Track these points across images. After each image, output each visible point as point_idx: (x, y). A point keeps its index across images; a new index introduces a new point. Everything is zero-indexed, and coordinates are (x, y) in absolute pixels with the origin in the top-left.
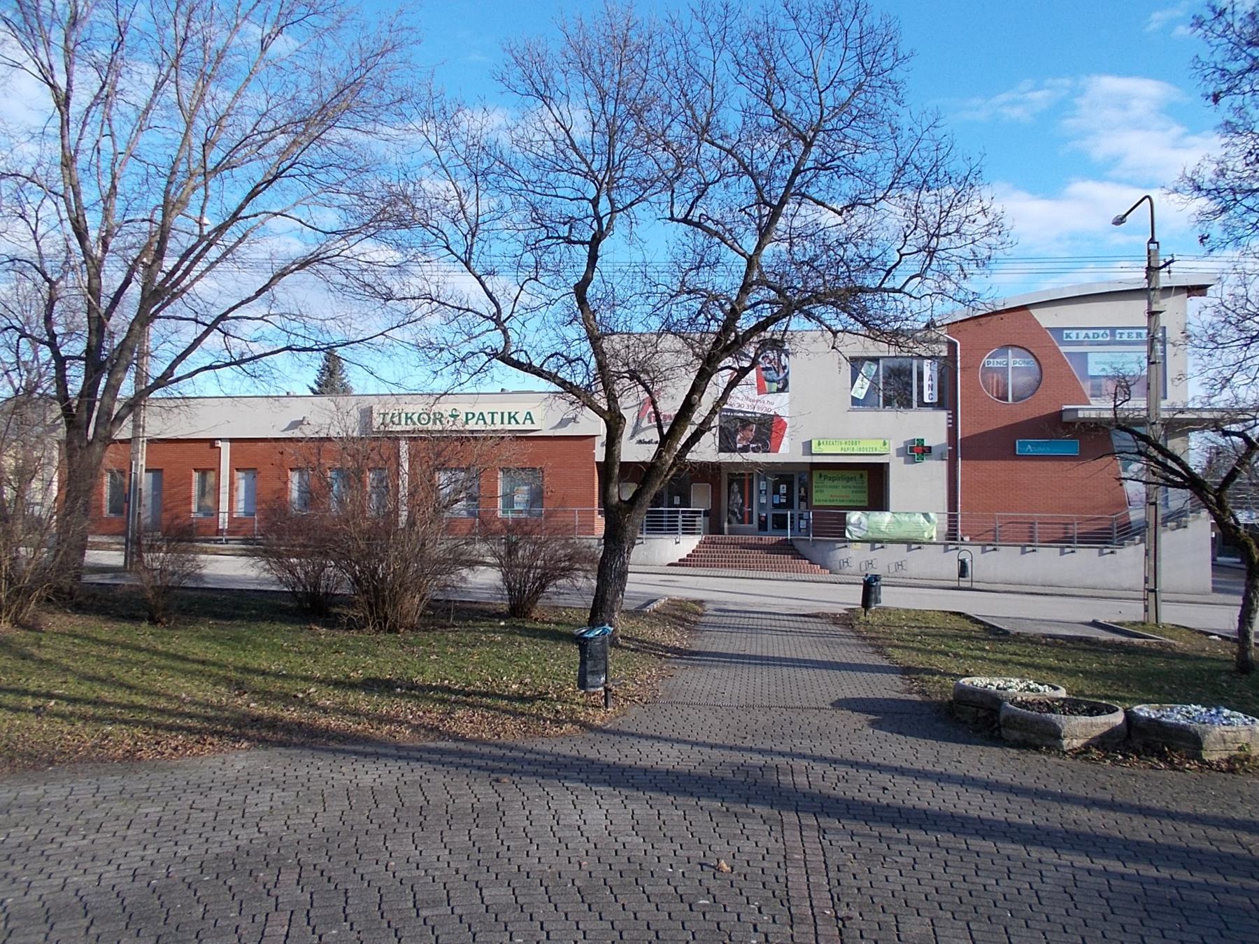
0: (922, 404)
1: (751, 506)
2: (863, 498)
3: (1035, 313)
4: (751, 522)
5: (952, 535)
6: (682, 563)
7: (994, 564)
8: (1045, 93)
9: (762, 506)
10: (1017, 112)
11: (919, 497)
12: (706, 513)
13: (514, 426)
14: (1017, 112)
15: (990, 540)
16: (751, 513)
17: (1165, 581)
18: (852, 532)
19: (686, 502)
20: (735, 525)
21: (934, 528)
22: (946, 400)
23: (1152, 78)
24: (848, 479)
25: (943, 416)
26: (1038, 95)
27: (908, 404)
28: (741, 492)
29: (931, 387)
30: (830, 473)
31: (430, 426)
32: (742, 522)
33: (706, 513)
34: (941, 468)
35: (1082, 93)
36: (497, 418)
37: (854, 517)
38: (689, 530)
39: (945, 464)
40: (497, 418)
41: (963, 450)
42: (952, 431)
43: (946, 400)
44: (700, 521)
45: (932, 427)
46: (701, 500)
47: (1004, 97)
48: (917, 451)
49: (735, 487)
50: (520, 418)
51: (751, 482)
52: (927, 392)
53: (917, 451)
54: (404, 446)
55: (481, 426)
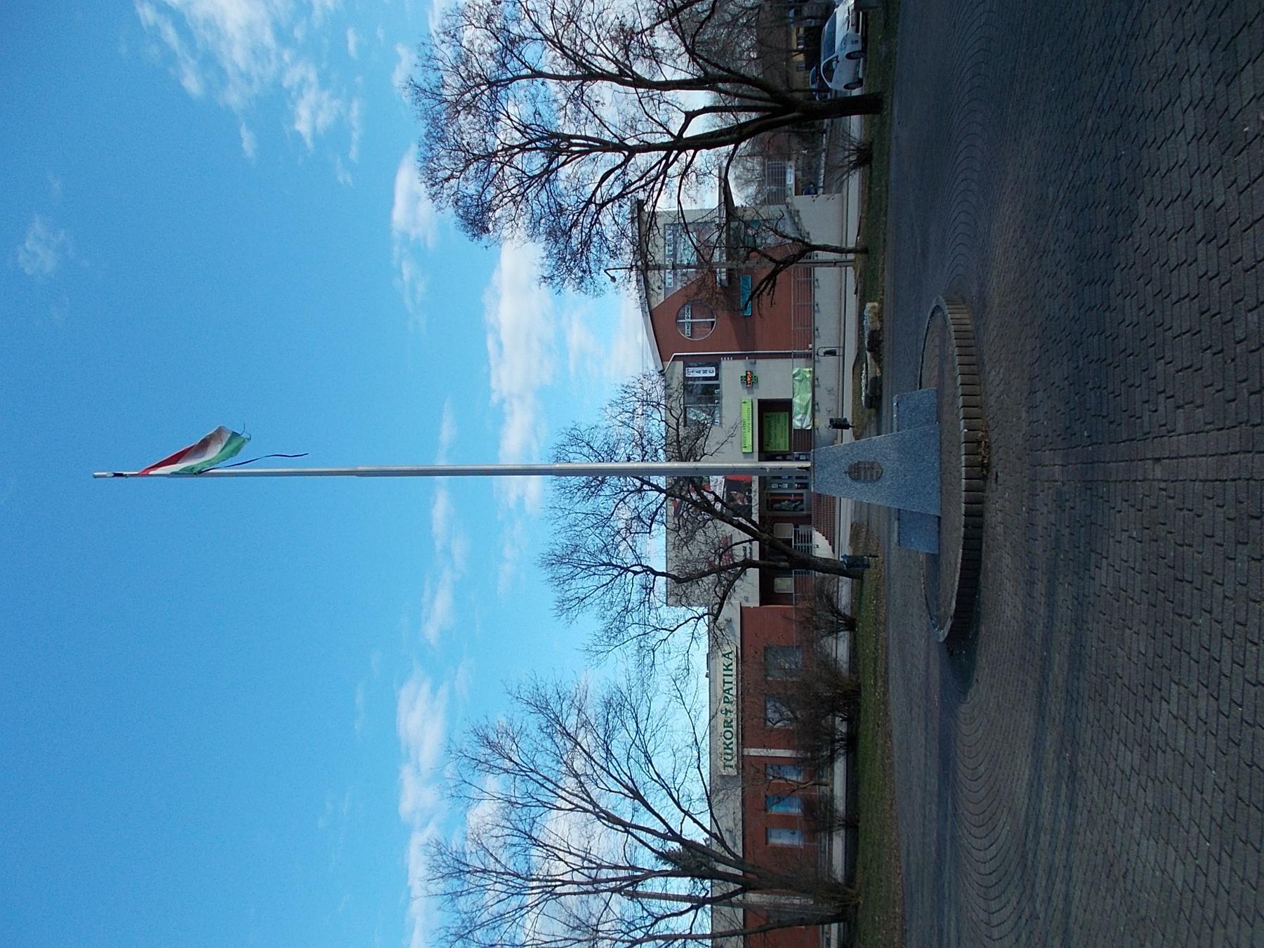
0: (716, 378)
1: (790, 495)
2: (783, 416)
3: (654, 305)
4: (802, 495)
5: (808, 356)
6: (832, 543)
7: (826, 337)
8: (404, 265)
9: (790, 486)
10: (421, 288)
11: (782, 378)
12: (796, 526)
13: (734, 667)
14: (421, 288)
15: (810, 333)
16: (795, 495)
17: (835, 244)
18: (807, 424)
19: (788, 542)
20: (804, 506)
21: (800, 368)
22: (715, 362)
23: (395, 175)
24: (770, 426)
25: (725, 363)
26: (406, 271)
27: (717, 387)
28: (779, 501)
29: (705, 372)
30: (766, 437)
31: (734, 730)
32: (802, 501)
33: (796, 526)
34: (761, 363)
35: (406, 235)
36: (728, 679)
37: (797, 424)
38: (809, 538)
39: (758, 361)
40: (728, 679)
41: (749, 348)
42: (735, 357)
43: (715, 362)
44: (802, 529)
45: (732, 370)
46: (787, 531)
47: (408, 302)
48: (750, 381)
49: (777, 506)
50: (727, 662)
51: (772, 495)
52: (708, 375)
53: (750, 381)
54: (753, 752)
55: (733, 692)
